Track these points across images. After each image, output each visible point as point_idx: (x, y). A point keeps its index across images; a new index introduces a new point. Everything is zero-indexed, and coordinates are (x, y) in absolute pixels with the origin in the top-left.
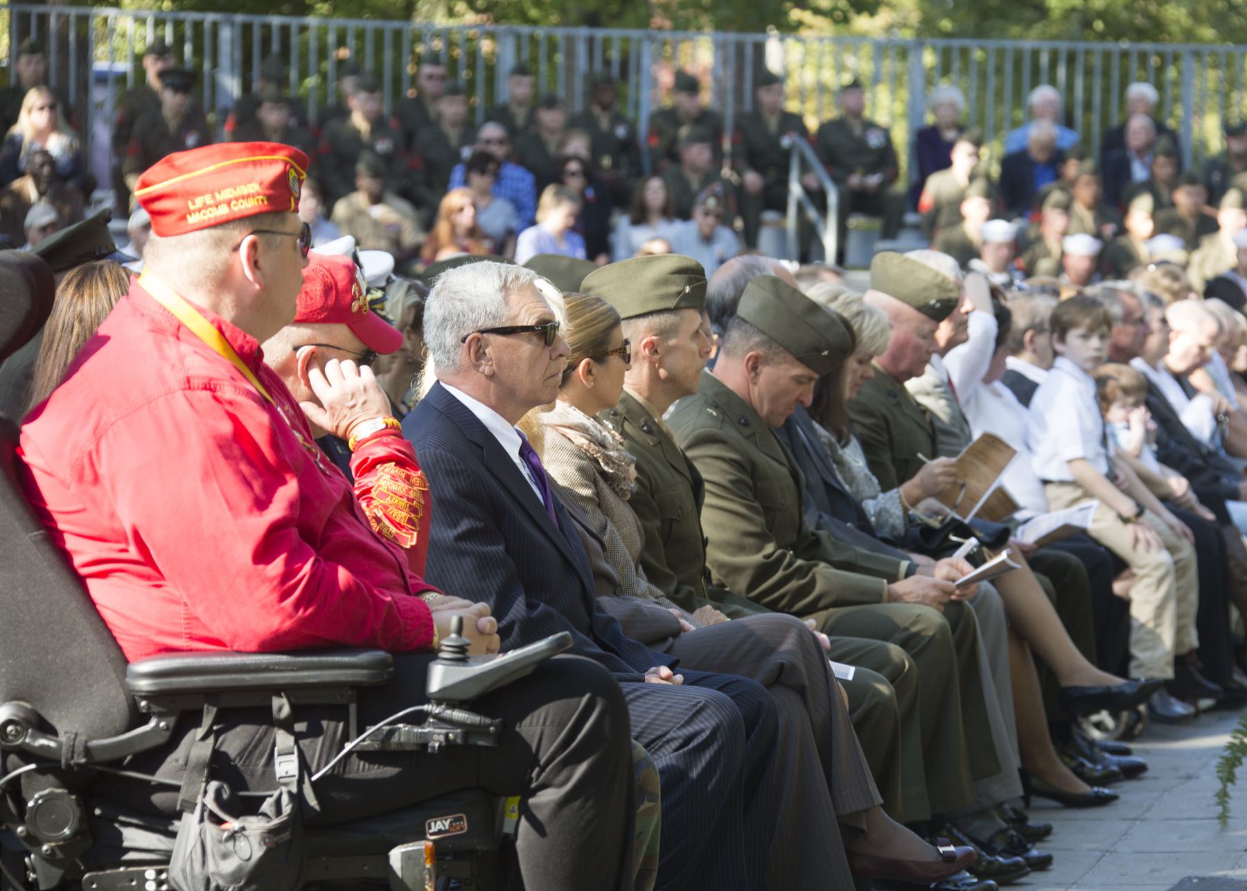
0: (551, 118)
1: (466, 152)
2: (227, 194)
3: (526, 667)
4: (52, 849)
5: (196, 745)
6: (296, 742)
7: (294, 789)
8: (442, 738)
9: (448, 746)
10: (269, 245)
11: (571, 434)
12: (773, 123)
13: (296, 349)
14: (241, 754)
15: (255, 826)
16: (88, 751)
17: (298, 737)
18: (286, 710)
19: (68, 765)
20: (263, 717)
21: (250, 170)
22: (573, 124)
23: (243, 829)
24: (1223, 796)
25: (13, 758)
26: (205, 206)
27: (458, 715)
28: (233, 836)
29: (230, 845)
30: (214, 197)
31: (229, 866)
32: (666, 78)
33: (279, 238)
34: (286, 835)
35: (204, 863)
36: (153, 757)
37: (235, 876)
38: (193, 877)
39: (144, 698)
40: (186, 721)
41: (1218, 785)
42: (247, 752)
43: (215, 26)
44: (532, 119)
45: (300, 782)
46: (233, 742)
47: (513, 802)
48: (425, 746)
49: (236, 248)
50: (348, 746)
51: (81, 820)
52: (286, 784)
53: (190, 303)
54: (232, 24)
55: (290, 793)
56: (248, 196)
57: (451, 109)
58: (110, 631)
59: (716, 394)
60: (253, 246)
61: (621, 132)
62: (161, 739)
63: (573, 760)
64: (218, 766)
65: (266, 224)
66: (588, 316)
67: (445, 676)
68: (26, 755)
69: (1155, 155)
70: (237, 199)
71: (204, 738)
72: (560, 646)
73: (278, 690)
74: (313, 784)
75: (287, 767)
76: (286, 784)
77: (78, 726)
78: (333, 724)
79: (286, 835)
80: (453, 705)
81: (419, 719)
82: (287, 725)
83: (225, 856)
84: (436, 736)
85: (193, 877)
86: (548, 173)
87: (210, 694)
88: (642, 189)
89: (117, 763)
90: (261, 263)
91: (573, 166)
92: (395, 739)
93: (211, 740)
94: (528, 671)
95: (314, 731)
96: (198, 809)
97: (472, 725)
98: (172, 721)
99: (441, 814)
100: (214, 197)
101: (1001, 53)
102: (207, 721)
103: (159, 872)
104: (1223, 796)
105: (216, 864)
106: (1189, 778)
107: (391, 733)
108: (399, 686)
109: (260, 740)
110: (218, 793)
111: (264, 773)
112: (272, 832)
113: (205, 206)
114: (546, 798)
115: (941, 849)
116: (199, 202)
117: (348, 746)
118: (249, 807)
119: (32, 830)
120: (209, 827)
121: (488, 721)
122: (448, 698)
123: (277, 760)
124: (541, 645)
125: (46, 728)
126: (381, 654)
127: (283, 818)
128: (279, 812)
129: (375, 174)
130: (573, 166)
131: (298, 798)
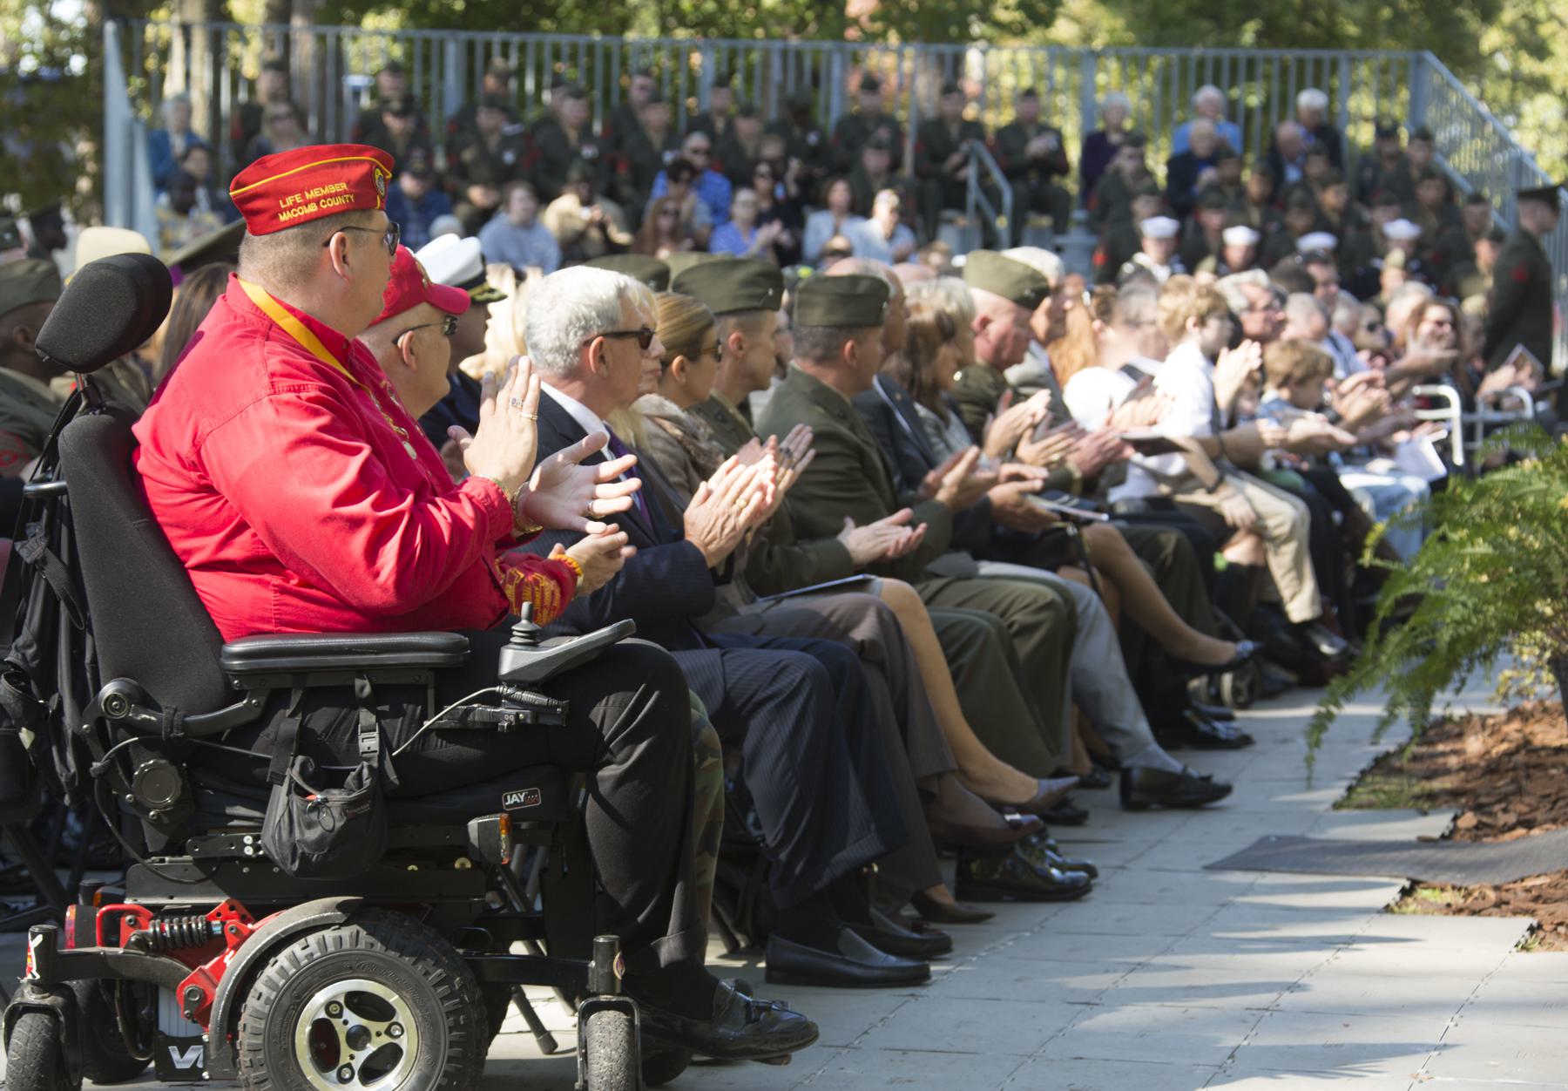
0: (745, 126)
1: (668, 157)
2: (314, 193)
3: (589, 652)
4: (158, 815)
5: (285, 723)
6: (378, 720)
7: (375, 764)
8: (512, 718)
9: (519, 725)
10: (356, 241)
11: (667, 424)
12: (954, 130)
13: (395, 341)
14: (326, 731)
15: (337, 796)
16: (185, 726)
17: (380, 716)
18: (368, 690)
19: (168, 738)
20: (345, 698)
21: (337, 171)
22: (770, 130)
23: (326, 800)
24: (1309, 761)
25: (122, 732)
26: (295, 205)
27: (527, 696)
28: (317, 807)
29: (314, 816)
30: (303, 197)
31: (312, 835)
32: (854, 82)
33: (365, 235)
34: (366, 807)
35: (291, 831)
36: (247, 731)
37: (319, 844)
38: (281, 843)
39: (236, 677)
40: (276, 700)
41: (1306, 750)
42: (333, 729)
43: (442, 44)
44: (730, 126)
45: (381, 758)
46: (321, 720)
47: (580, 775)
48: (496, 724)
49: (327, 244)
50: (427, 724)
51: (183, 788)
52: (368, 760)
53: (280, 302)
54: (456, 41)
55: (370, 768)
56: (336, 195)
57: (655, 117)
58: (208, 615)
59: (814, 392)
60: (342, 242)
61: (812, 138)
62: (251, 717)
63: (633, 740)
64: (304, 742)
65: (354, 219)
66: (684, 316)
67: (514, 661)
68: (132, 727)
69: (631, 76)
70: (325, 197)
71: (292, 715)
72: (621, 633)
73: (361, 671)
74: (393, 759)
75: (369, 743)
76: (368, 760)
77: (177, 705)
78: (411, 707)
79: (366, 807)
80: (523, 687)
81: (494, 700)
82: (370, 704)
83: (310, 825)
84: (507, 715)
85: (281, 843)
86: (741, 177)
87: (299, 674)
88: (828, 190)
89: (216, 737)
90: (350, 258)
91: (763, 168)
92: (470, 718)
93: (299, 718)
94: (593, 656)
95: (397, 712)
96: (287, 780)
97: (540, 706)
98: (263, 700)
99: (516, 788)
100: (303, 197)
101: (1184, 61)
102: (295, 699)
103: (256, 838)
104: (1309, 761)
105: (302, 833)
106: (1285, 741)
107: (467, 712)
108: (474, 668)
109: (345, 717)
110: (303, 766)
111: (348, 749)
112: (351, 804)
113: (295, 205)
114: (610, 772)
115: (1008, 818)
116: (289, 201)
117: (427, 724)
118: (336, 781)
119: (139, 798)
120: (296, 799)
121: (555, 702)
122: (519, 680)
123: (361, 736)
124: (604, 631)
125: (147, 703)
126: (457, 637)
127: (363, 791)
128: (360, 785)
129: (586, 179)
130: (763, 168)
131: (378, 773)
